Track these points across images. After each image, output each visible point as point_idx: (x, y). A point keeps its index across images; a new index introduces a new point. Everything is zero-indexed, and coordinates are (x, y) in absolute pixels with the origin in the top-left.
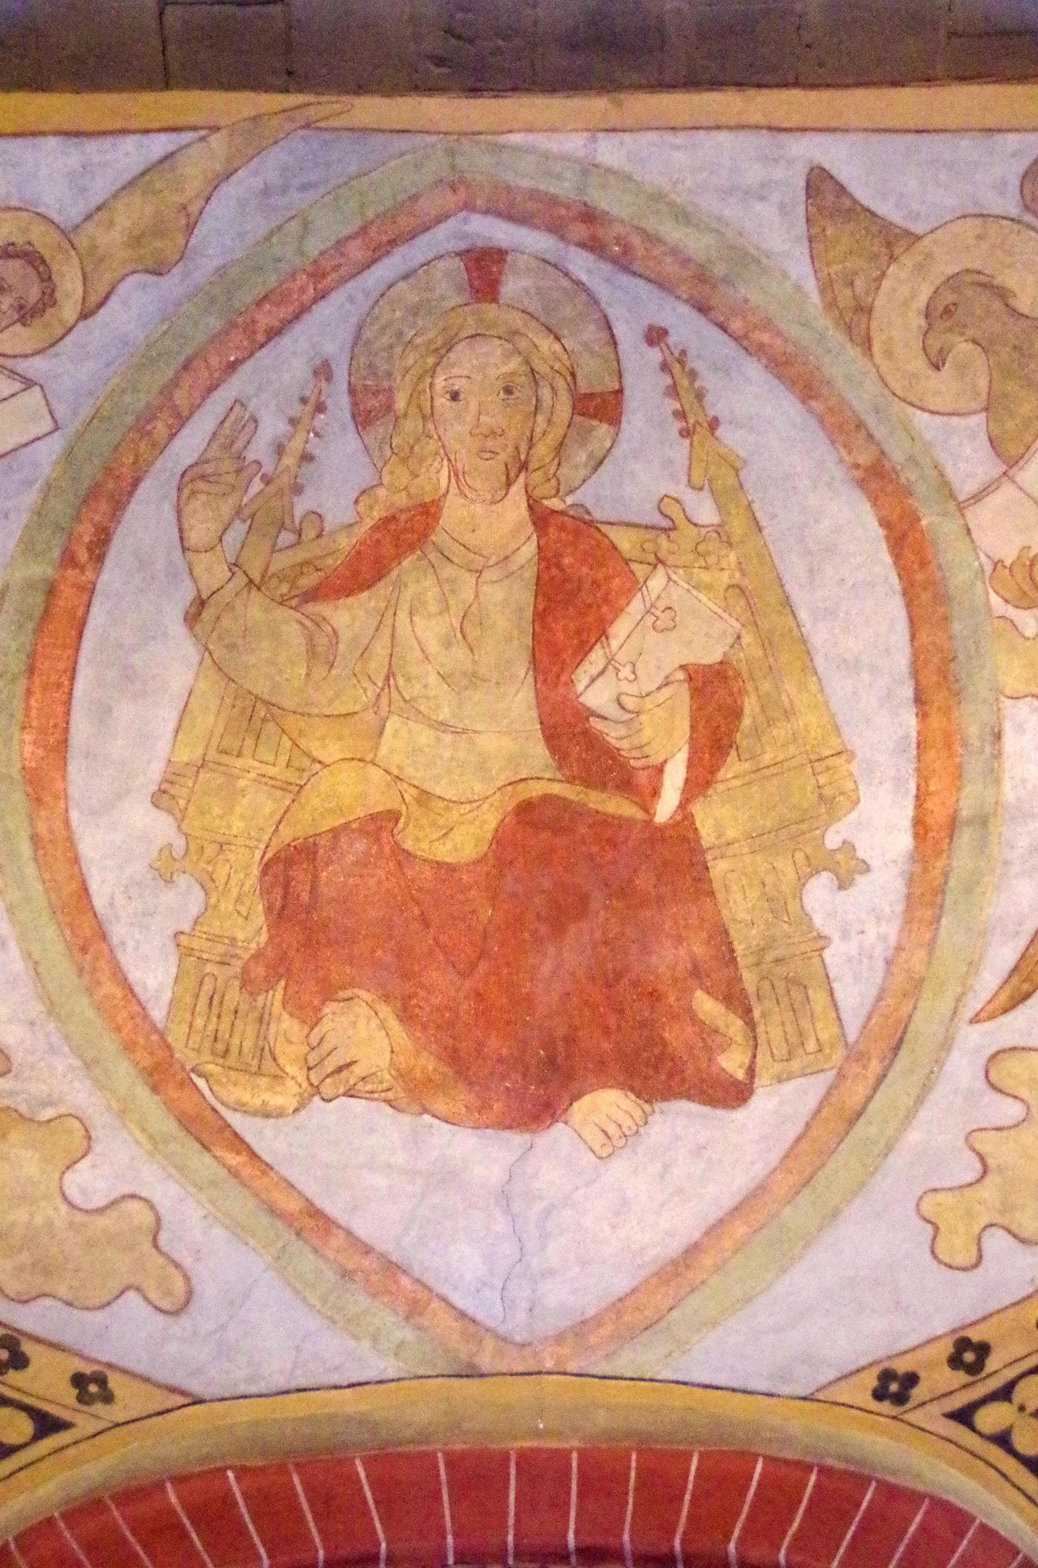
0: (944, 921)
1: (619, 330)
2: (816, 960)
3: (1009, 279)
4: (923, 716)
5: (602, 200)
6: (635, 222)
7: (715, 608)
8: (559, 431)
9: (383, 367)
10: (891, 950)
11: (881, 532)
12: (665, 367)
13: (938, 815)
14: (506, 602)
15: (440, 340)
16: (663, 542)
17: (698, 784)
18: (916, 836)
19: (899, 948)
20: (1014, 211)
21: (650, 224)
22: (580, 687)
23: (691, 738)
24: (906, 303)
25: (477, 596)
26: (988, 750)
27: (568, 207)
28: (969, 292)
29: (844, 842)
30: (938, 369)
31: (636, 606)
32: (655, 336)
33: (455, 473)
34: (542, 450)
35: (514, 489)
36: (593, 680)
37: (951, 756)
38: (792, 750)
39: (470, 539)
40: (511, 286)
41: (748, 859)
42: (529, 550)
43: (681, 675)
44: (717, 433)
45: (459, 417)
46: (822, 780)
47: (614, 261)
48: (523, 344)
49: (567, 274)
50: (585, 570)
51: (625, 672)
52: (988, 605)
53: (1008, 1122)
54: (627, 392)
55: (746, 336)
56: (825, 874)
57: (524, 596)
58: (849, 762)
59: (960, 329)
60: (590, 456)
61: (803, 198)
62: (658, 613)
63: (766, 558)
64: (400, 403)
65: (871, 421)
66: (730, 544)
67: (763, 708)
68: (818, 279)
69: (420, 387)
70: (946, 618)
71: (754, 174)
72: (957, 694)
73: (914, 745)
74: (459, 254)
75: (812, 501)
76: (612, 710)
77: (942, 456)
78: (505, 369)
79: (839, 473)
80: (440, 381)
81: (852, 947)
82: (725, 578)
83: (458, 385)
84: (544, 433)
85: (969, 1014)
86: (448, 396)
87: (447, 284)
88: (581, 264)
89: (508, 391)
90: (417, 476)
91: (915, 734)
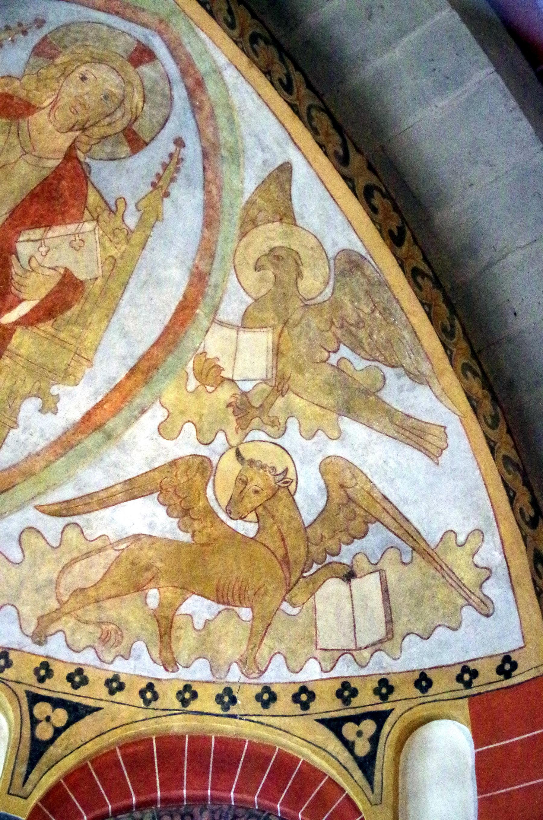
0: (63, 459)
1: (169, 125)
2: (6, 430)
3: (306, 273)
4: (128, 377)
5: (211, 86)
6: (213, 104)
7: (99, 259)
8: (110, 131)
9: (66, 41)
10: (34, 452)
11: (181, 298)
12: (171, 155)
13: (97, 418)
14: (25, 175)
15: (98, 57)
16: (106, 213)
17: (28, 321)
18: (83, 418)
19: (38, 454)
20: (331, 254)
21: (218, 111)
22: (21, 239)
23: (42, 300)
24: (269, 238)
25: (15, 162)
26: (136, 413)
27: (196, 72)
28: (291, 261)
29: (58, 395)
30: (256, 270)
31: (72, 228)
32: (179, 143)
33: (54, 104)
34: (97, 131)
35: (70, 134)
36: (28, 241)
37: (122, 402)
38: (73, 341)
39: (34, 134)
40: (146, 69)
41: (19, 367)
42: (52, 164)
43: (62, 271)
44: (164, 199)
45: (76, 87)
46: (73, 364)
47: (193, 106)
48: (129, 88)
49: (171, 89)
50: (67, 194)
51: (43, 249)
52: (186, 365)
53: (11, 558)
54: (148, 147)
55: (209, 182)
56: (40, 399)
57: (33, 181)
58: (88, 367)
59: (276, 266)
60: (112, 153)
61: (276, 167)
62: (77, 238)
63: (135, 260)
64: (58, 61)
65: (217, 259)
66: (128, 241)
67: (78, 315)
68: (251, 197)
69: (73, 63)
70: (170, 352)
71: (268, 140)
72: (146, 382)
73: (114, 384)
74: (138, 41)
75: (171, 260)
76: (24, 259)
77: (225, 298)
78: (113, 90)
79: (189, 264)
80: (83, 69)
81: (23, 437)
82: (114, 252)
83: (90, 77)
84: (103, 126)
85: (37, 503)
86: (81, 76)
87: (123, 45)
88: (179, 93)
89: (106, 97)
90: (37, 90)
91: (118, 381)
